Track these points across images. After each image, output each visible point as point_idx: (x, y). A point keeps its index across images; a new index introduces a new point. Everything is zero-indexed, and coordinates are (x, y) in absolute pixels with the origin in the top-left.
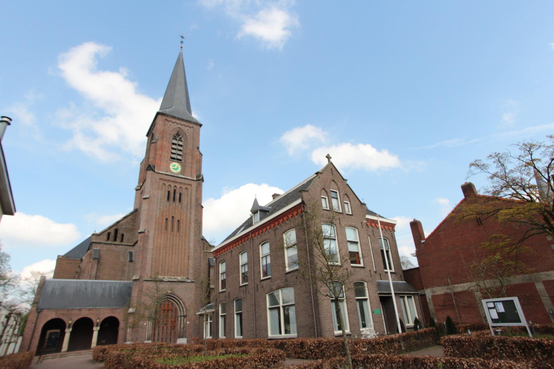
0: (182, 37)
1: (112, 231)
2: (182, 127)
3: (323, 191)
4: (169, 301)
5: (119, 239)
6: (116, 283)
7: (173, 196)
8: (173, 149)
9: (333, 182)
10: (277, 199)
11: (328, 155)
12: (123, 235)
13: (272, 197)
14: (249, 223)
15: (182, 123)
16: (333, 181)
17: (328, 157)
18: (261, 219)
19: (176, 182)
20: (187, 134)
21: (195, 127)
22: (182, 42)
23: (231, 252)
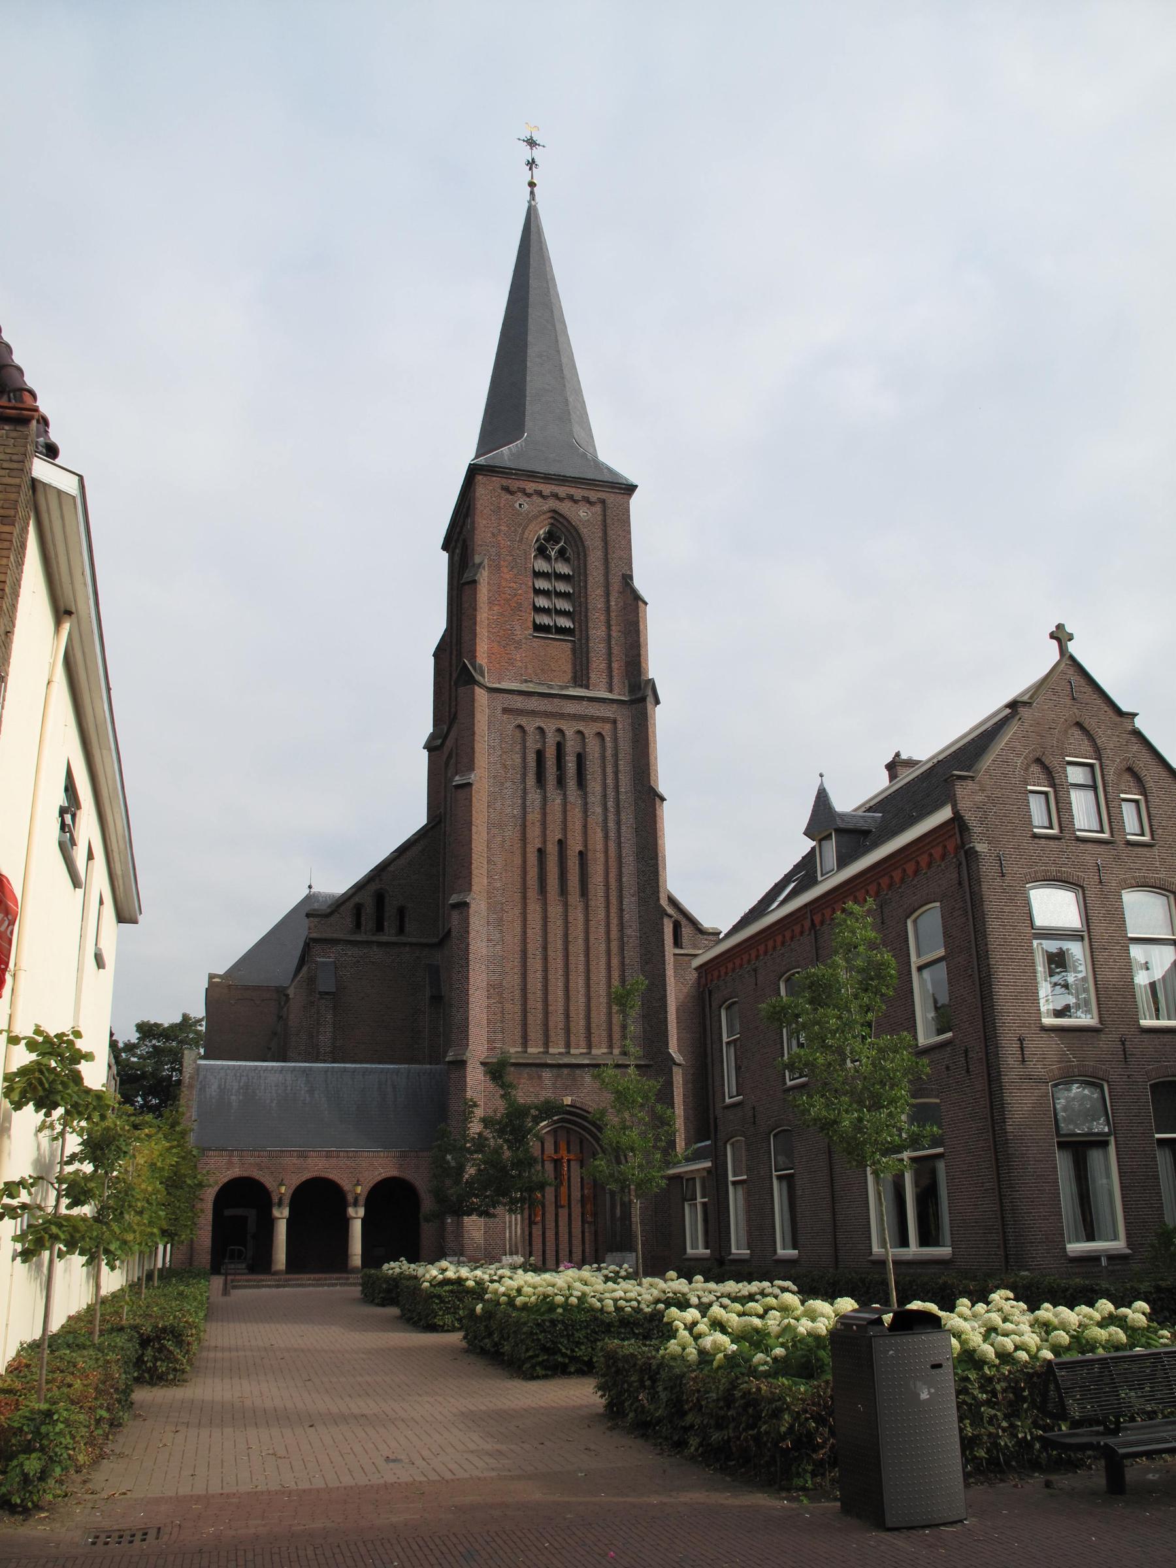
0: (532, 143)
1: (368, 900)
2: (565, 508)
3: (1035, 769)
4: (568, 1130)
5: (390, 925)
6: (398, 1071)
7: (551, 767)
8: (538, 592)
9: (1077, 732)
10: (906, 776)
11: (1060, 627)
12: (401, 912)
13: (886, 773)
14: (804, 872)
15: (562, 491)
16: (1079, 725)
17: (1060, 636)
18: (843, 862)
19: (562, 716)
20: (584, 531)
21: (611, 498)
22: (531, 164)
23: (755, 970)
